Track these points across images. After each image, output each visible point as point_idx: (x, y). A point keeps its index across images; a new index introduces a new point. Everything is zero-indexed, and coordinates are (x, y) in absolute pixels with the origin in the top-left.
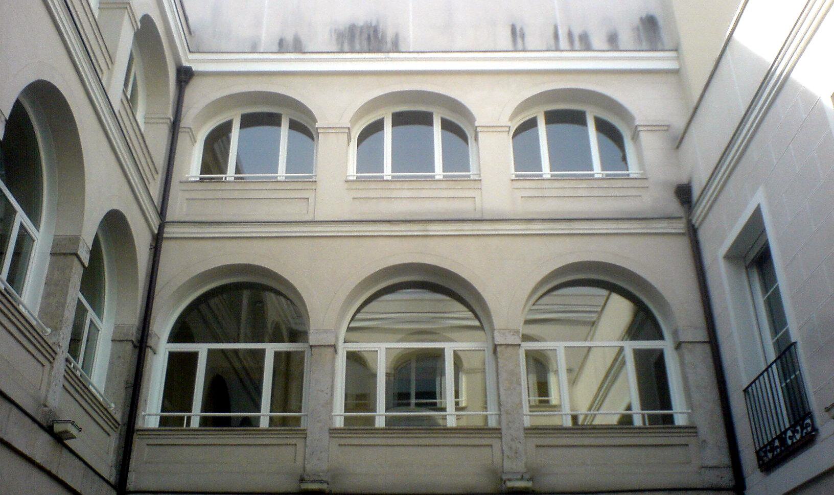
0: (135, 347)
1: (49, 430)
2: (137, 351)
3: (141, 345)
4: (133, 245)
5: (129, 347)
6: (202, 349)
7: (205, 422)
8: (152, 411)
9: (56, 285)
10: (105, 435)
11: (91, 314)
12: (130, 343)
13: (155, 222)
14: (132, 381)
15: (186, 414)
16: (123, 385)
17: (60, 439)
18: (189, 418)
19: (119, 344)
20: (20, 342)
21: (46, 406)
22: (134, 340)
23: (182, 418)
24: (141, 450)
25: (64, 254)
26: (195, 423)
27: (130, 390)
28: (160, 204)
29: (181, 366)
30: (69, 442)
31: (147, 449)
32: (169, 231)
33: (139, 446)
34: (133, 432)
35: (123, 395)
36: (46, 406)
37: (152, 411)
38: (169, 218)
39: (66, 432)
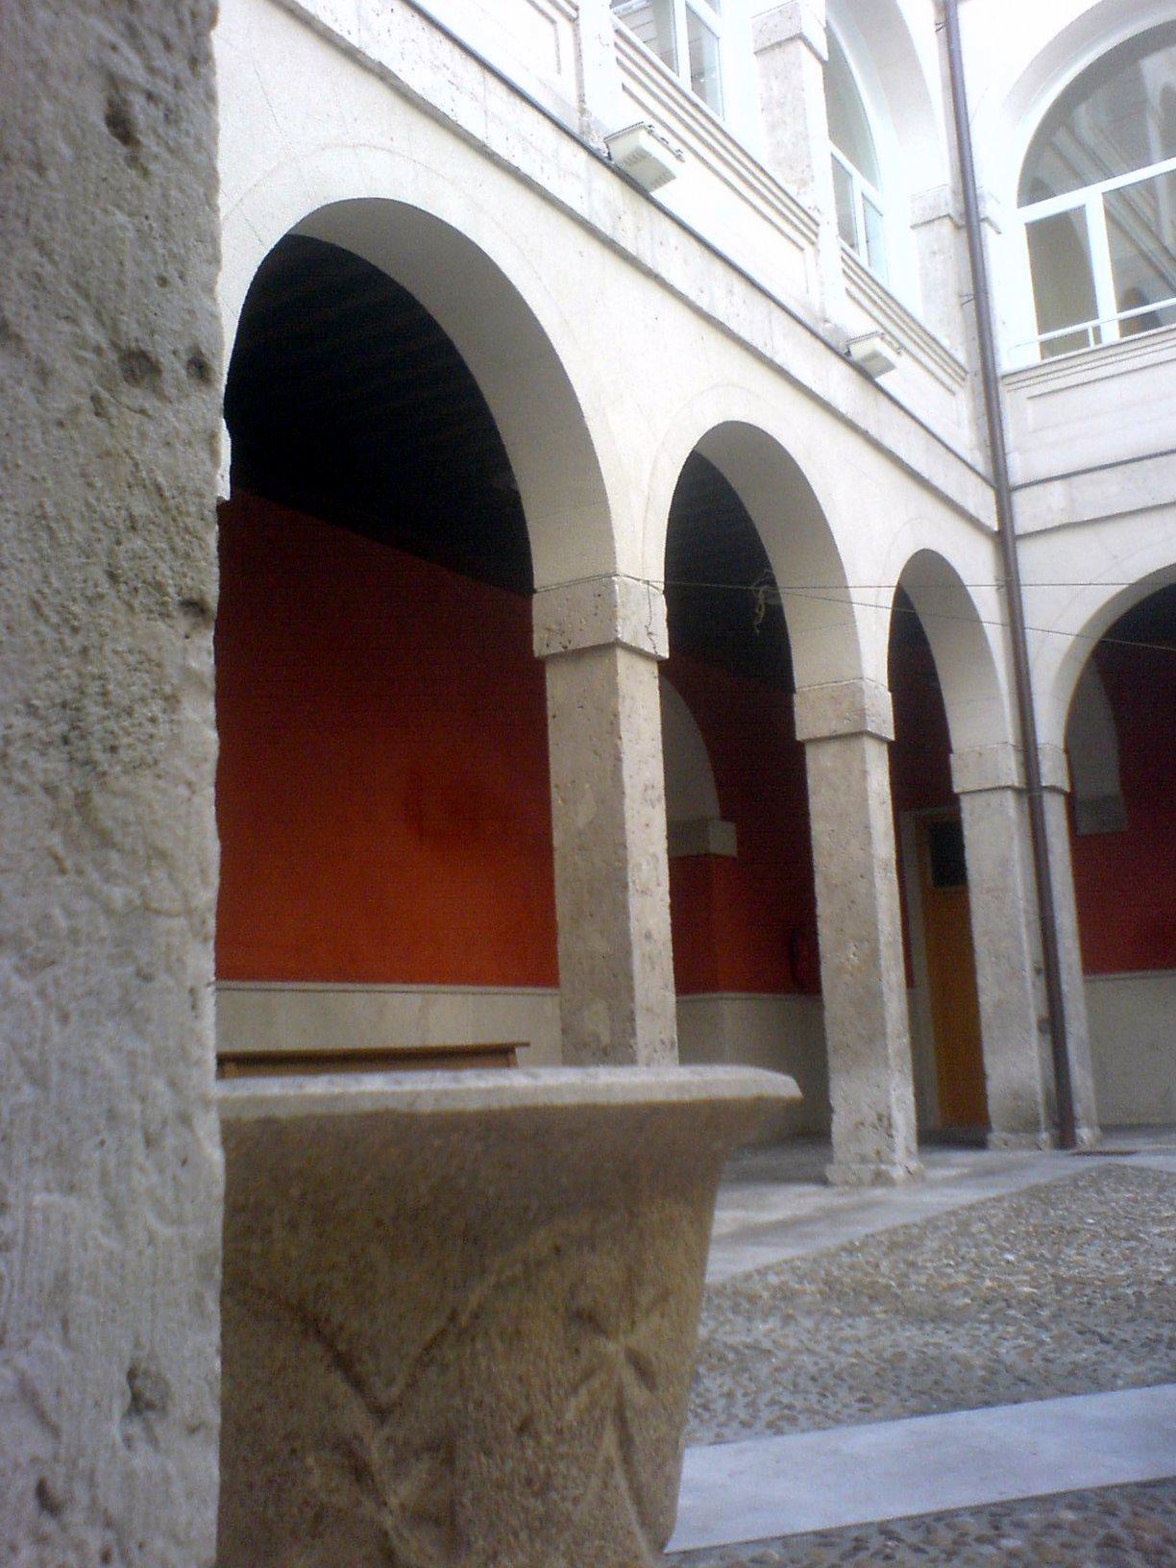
0: (958, 227)
1: (845, 357)
2: (964, 234)
3: (969, 221)
4: (902, 24)
5: (946, 228)
6: (1089, 200)
7: (1128, 327)
8: (1018, 334)
9: (781, 105)
10: (947, 395)
11: (859, 183)
12: (947, 221)
13: (982, 502)
14: (968, 288)
15: (1089, 325)
16: (954, 300)
17: (866, 372)
18: (1097, 330)
19: (924, 230)
20: (755, 207)
21: (826, 321)
22: (951, 212)
23: (1085, 332)
24: (1016, 409)
25: (779, 44)
26: (1111, 333)
27: (971, 307)
28: (990, 468)
29: (1056, 248)
30: (881, 380)
31: (1029, 403)
32: (1028, 513)
33: (1011, 402)
34: (996, 381)
35: (959, 319)
36: (826, 321)
37: (1018, 334)
38: (1018, 468)
39: (875, 356)
